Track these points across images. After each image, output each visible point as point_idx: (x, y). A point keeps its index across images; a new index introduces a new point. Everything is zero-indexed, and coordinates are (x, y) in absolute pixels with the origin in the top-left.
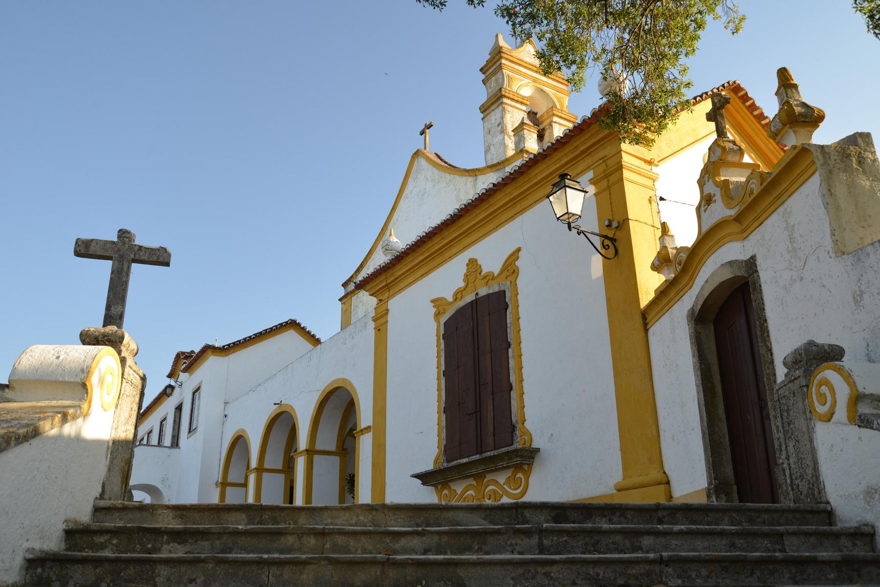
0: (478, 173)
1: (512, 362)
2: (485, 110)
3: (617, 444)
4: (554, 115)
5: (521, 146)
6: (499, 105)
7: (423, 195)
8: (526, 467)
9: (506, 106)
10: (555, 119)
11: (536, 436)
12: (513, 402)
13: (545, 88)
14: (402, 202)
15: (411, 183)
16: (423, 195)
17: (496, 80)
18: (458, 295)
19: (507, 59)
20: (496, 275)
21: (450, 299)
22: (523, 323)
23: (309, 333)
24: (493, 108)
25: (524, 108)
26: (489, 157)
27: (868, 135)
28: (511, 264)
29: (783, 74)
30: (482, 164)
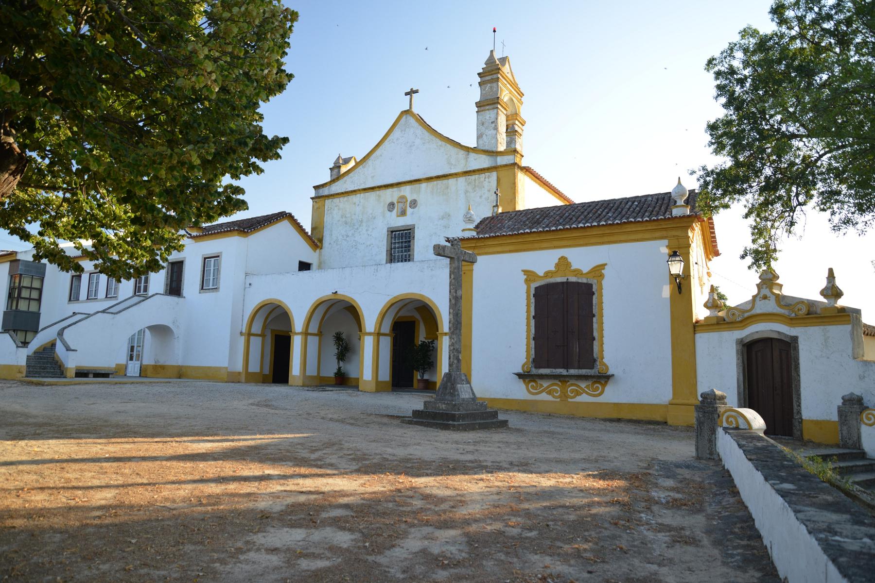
0: (470, 150)
1: (595, 326)
2: (480, 107)
3: (670, 382)
4: (517, 119)
5: (513, 146)
6: (494, 108)
7: (411, 146)
8: (603, 382)
9: (500, 112)
10: (517, 122)
11: (169, 232)
12: (595, 347)
13: (514, 99)
14: (386, 143)
15: (397, 133)
16: (411, 146)
17: (491, 87)
18: (548, 274)
19: (501, 75)
20: (572, 268)
21: (541, 274)
22: (605, 306)
23: (298, 224)
24: (487, 107)
25: (505, 112)
26: (481, 142)
27: (860, 310)
28: (598, 270)
29: (831, 271)
30: (472, 144)
